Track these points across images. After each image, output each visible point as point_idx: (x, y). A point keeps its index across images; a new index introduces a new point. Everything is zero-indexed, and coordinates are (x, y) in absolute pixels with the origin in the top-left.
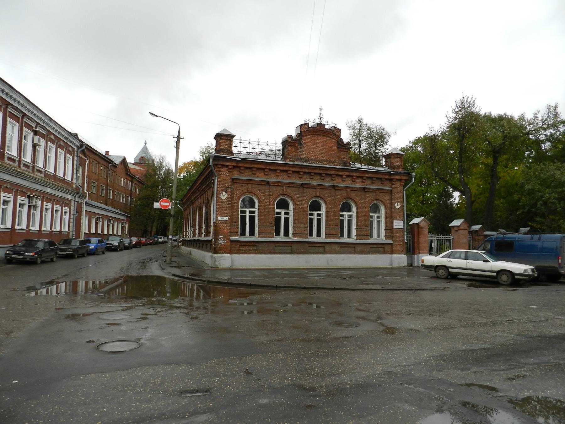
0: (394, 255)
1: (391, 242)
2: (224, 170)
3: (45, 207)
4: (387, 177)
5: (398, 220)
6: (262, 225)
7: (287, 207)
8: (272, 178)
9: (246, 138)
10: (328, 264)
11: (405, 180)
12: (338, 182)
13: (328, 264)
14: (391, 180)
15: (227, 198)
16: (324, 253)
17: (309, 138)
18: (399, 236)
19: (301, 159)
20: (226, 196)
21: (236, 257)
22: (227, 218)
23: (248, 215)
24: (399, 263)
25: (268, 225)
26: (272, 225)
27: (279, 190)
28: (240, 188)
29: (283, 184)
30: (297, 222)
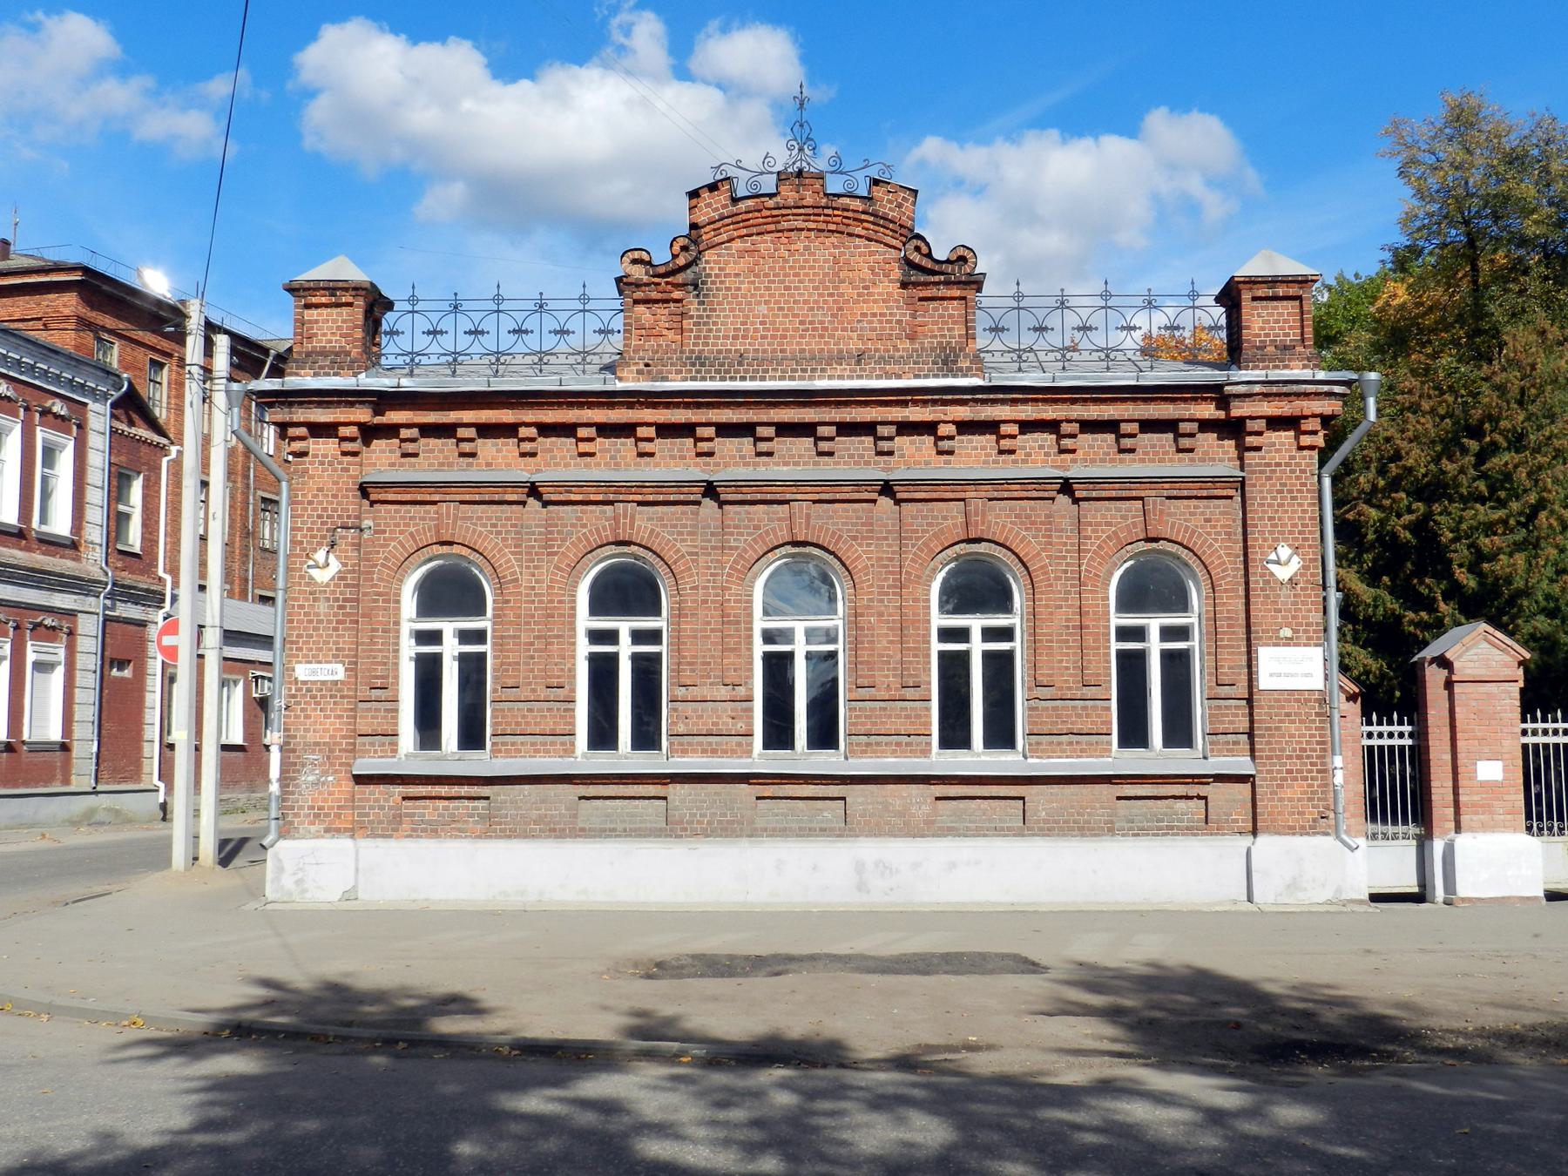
0: (1266, 845)
1: (1241, 763)
2: (325, 447)
3: (31, 657)
4: (1208, 411)
5: (1288, 642)
6: (863, 693)
7: (1003, 602)
8: (558, 462)
9: (434, 294)
10: (861, 887)
11: (1326, 420)
12: (914, 459)
13: (861, 887)
14: (1232, 429)
15: (341, 577)
16: (847, 829)
17: (741, 253)
18: (1296, 733)
19: (699, 363)
20: (335, 566)
21: (375, 851)
22: (338, 672)
23: (1155, 647)
24: (1293, 886)
25: (543, 693)
26: (741, 692)
27: (597, 520)
28: (401, 526)
29: (608, 494)
30: (687, 675)
